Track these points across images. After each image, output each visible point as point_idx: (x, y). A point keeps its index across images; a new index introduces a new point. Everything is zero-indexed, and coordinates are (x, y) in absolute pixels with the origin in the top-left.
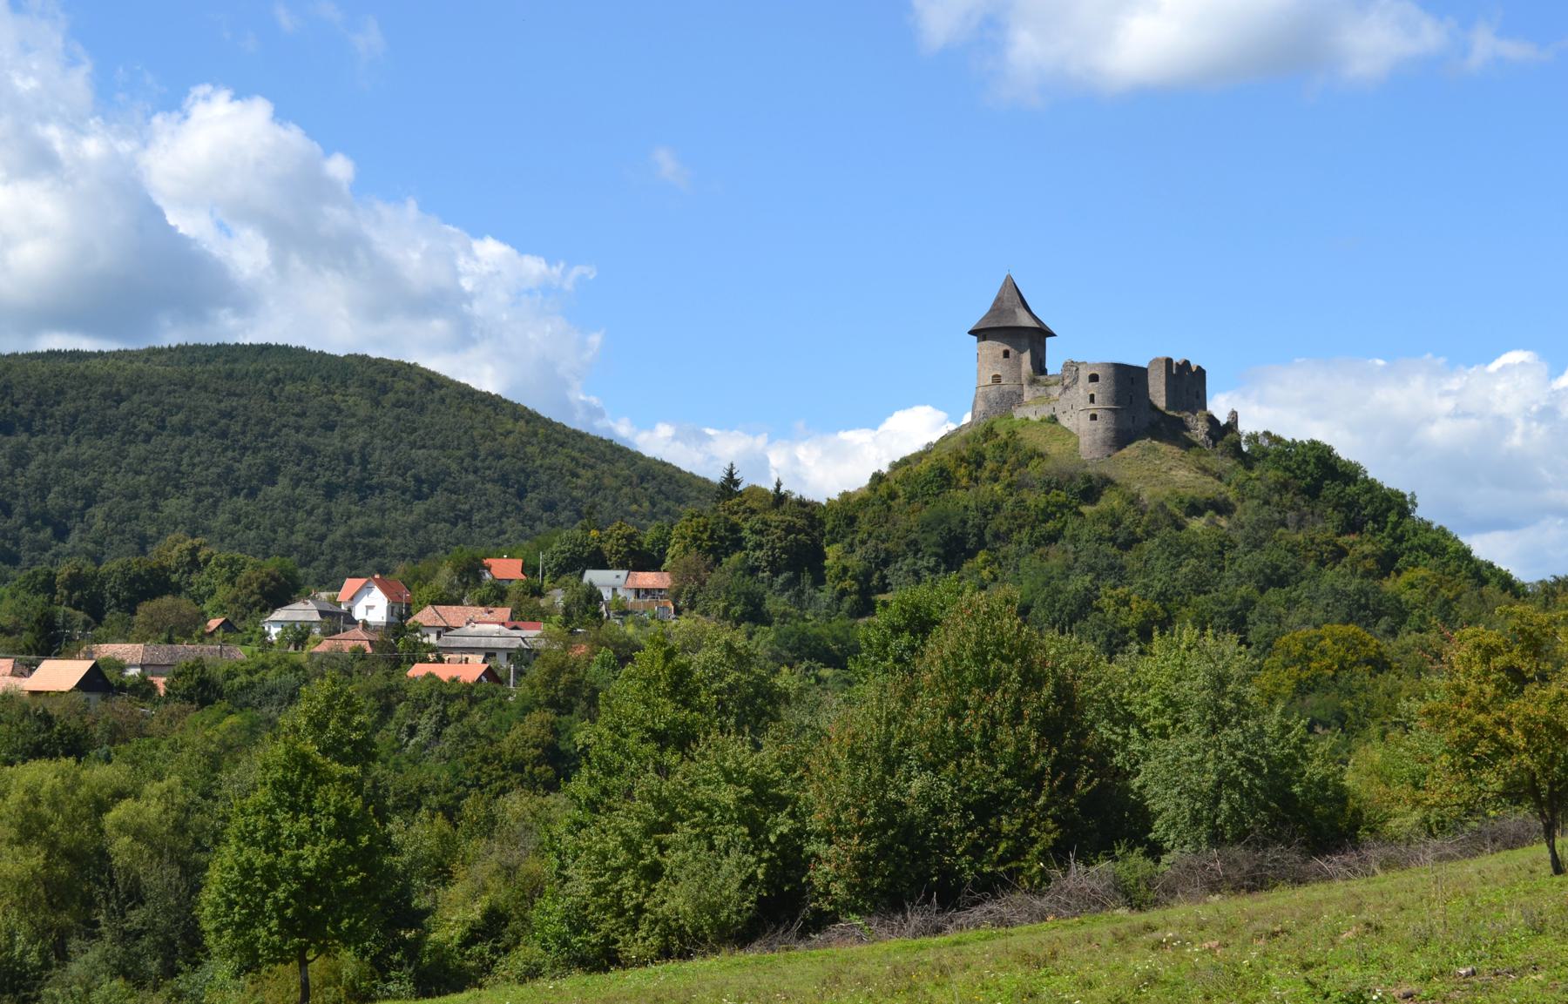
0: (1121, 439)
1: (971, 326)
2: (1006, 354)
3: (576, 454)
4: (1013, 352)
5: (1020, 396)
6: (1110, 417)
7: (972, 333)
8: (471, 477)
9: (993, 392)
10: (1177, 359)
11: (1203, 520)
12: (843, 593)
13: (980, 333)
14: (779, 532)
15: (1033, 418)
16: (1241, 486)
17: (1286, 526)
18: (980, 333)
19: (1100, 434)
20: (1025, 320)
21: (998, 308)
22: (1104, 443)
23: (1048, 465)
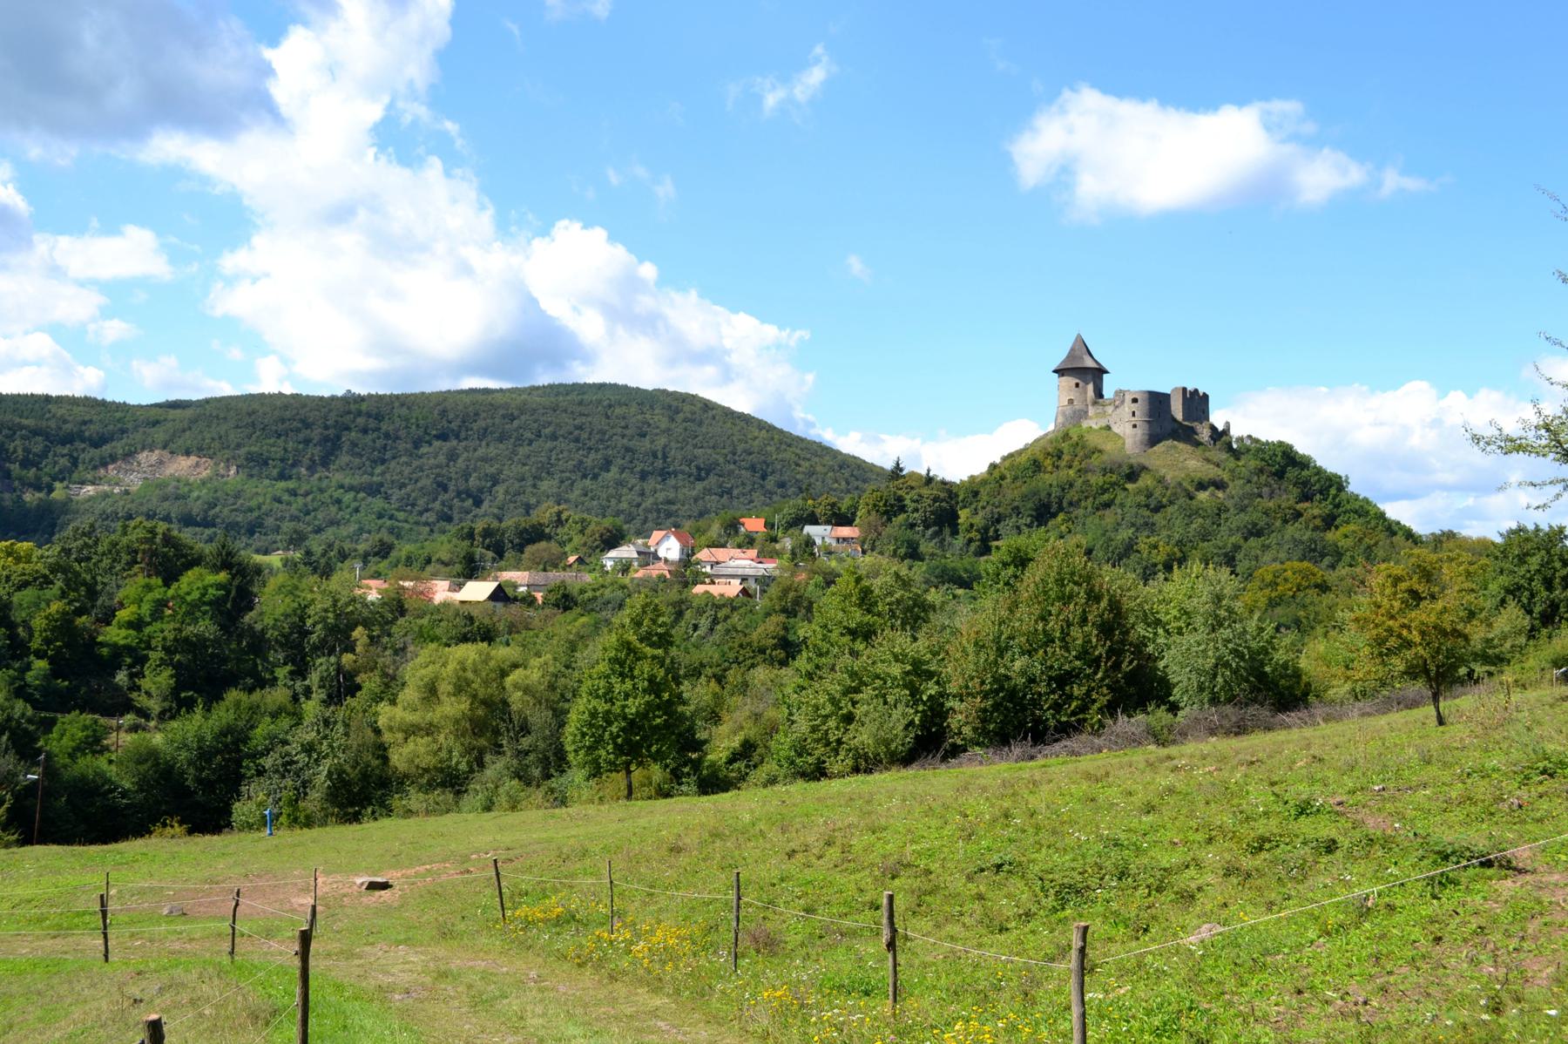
0: (1153, 440)
1: (1054, 367)
2: (1077, 385)
3: (798, 451)
4: (1081, 384)
5: (1086, 412)
6: (1146, 426)
7: (1055, 371)
8: (732, 467)
9: (1069, 410)
10: (1190, 388)
11: (1207, 493)
12: (970, 541)
13: (1060, 372)
14: (929, 501)
15: (1095, 427)
16: (1232, 471)
17: (1262, 497)
18: (1060, 372)
19: (1139, 437)
20: (1089, 363)
21: (1072, 355)
22: (1142, 443)
23: (1105, 457)
